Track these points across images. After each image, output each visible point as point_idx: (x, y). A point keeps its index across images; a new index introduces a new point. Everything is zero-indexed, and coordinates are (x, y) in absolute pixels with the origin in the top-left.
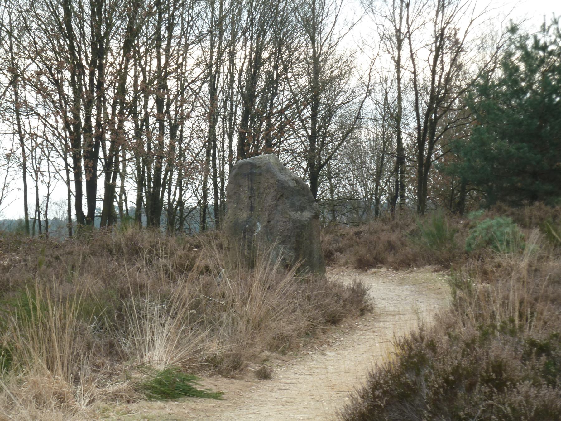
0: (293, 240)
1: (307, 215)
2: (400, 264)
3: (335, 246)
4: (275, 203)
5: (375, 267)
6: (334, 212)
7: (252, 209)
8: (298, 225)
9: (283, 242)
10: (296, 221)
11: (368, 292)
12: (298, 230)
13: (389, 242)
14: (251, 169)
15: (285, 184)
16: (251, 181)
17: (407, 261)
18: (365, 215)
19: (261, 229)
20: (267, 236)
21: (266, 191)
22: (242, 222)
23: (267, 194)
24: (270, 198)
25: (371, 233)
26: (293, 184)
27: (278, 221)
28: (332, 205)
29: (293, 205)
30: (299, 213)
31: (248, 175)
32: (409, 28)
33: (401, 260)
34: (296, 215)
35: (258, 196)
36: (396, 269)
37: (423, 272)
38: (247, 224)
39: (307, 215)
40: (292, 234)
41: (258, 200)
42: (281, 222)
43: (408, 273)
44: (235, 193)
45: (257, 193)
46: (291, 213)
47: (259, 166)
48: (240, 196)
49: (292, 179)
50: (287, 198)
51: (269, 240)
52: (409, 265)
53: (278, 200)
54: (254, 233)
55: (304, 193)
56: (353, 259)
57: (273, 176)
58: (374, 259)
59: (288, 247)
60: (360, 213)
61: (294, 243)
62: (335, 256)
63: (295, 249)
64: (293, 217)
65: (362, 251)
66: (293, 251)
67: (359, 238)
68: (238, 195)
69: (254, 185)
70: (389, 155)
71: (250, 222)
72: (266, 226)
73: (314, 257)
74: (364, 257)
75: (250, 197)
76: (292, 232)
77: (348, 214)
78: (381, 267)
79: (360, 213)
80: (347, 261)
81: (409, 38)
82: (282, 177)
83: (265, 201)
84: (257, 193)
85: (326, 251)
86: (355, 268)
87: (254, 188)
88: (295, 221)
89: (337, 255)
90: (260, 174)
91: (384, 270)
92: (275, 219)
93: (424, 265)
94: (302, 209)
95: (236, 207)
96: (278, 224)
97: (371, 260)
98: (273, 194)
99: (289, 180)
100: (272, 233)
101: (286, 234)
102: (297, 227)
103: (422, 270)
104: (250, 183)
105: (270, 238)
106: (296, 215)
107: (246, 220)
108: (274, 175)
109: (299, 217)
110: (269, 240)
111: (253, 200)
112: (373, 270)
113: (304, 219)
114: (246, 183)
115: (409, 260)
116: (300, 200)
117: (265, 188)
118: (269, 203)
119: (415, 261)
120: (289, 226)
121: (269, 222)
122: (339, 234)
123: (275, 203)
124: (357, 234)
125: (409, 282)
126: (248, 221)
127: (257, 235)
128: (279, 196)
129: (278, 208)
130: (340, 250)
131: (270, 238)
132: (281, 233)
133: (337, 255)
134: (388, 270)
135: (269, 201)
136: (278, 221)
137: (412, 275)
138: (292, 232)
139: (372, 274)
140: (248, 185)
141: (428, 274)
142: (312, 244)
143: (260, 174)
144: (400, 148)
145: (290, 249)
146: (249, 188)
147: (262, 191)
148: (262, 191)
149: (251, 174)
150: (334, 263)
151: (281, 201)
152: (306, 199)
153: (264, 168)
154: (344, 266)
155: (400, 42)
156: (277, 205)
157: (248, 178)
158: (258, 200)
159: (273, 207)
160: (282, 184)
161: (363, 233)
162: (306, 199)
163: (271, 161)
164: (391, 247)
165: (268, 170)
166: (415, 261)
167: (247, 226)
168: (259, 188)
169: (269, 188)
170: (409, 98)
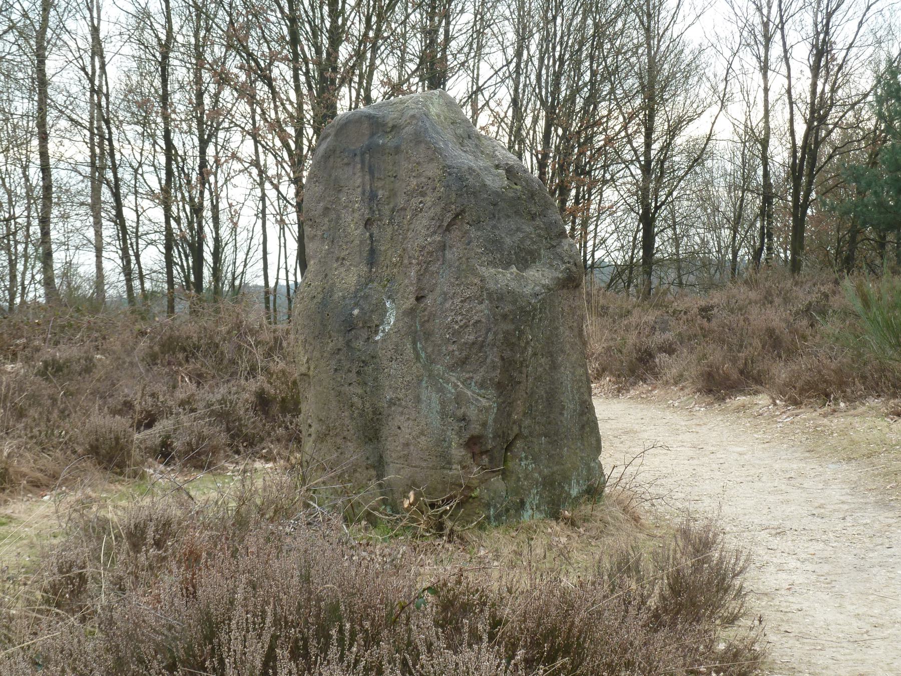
0: (493, 356)
1: (540, 277)
2: (802, 391)
3: (659, 338)
4: (438, 238)
5: (742, 392)
6: (679, 269)
7: (372, 257)
8: (508, 308)
9: (463, 362)
10: (501, 298)
11: (737, 583)
12: (511, 327)
13: (771, 332)
14: (373, 135)
15: (471, 180)
16: (371, 172)
17: (823, 386)
18: (718, 273)
19: (397, 321)
20: (414, 343)
21: (414, 202)
22: (344, 298)
23: (417, 212)
24: (425, 222)
25: (732, 311)
26: (496, 181)
27: (445, 296)
28: (676, 261)
29: (494, 245)
30: (514, 269)
31: (363, 154)
32: (781, 17)
33: (808, 383)
34: (505, 278)
35: (392, 218)
36: (796, 403)
37: (862, 415)
38: (356, 305)
39: (540, 277)
40: (490, 336)
41: (389, 230)
42: (457, 301)
43: (825, 416)
44: (326, 209)
45: (386, 210)
46: (488, 272)
47: (394, 127)
48: (339, 218)
49: (497, 167)
50: (477, 223)
51: (418, 357)
52: (827, 395)
53: (448, 229)
54: (376, 332)
55: (534, 209)
56: (694, 371)
57: (435, 153)
58: (742, 372)
59: (478, 377)
60: (712, 271)
61: (494, 368)
62: (657, 360)
63: (500, 386)
64: (491, 286)
65: (716, 355)
66: (492, 392)
67: (709, 320)
68: (333, 216)
69: (380, 184)
70: (752, 192)
71: (366, 297)
72: (411, 312)
73: (563, 408)
74: (718, 369)
75: (368, 223)
76: (489, 330)
77: (697, 272)
78: (756, 393)
79: (712, 271)
80: (682, 376)
81: (782, 29)
82: (464, 159)
83: (410, 235)
84: (386, 210)
85: (640, 350)
86: (699, 391)
87: (380, 193)
88: (497, 298)
89: (661, 358)
90: (397, 150)
91: (763, 400)
92: (438, 290)
93: (863, 397)
94: (524, 258)
95: (329, 252)
96: (447, 305)
97: (735, 375)
98: (431, 213)
99: (486, 169)
100: (428, 335)
101: (472, 338)
102: (505, 317)
103: (861, 409)
104: (367, 177)
105: (424, 349)
106: (505, 278)
107: (357, 291)
108: (437, 150)
109: (513, 285)
110: (418, 357)
111: (375, 230)
112: (741, 399)
113: (528, 290)
114: (355, 179)
115: (826, 381)
116: (518, 230)
117: (410, 195)
118: (420, 241)
119: (842, 385)
120: (482, 310)
121: (419, 299)
122: (671, 311)
123: (438, 238)
124: (705, 311)
125: (835, 450)
126: (359, 295)
127: (384, 340)
128: (449, 217)
129: (449, 255)
130: (669, 350)
131: (424, 349)
132: (455, 333)
133: (661, 358)
134: (775, 404)
135: (420, 231)
136: (445, 296)
137: (837, 422)
138: (489, 330)
139: (738, 410)
140: (363, 184)
141: (881, 424)
142: (554, 366)
143: (397, 150)
144: (767, 185)
145: (482, 385)
146: (363, 193)
147: (401, 201)
148: (401, 201)
149: (371, 149)
150: (656, 378)
151: (455, 234)
152: (537, 228)
153: (409, 129)
154: (676, 384)
155: (768, 39)
156: (443, 247)
157: (363, 162)
158: (389, 230)
159: (430, 253)
160: (460, 179)
161: (716, 310)
162: (537, 228)
163: (434, 110)
164: (774, 343)
165: (419, 138)
166: (842, 385)
167: (356, 312)
168: (393, 194)
169: (423, 194)
170: (779, 119)
